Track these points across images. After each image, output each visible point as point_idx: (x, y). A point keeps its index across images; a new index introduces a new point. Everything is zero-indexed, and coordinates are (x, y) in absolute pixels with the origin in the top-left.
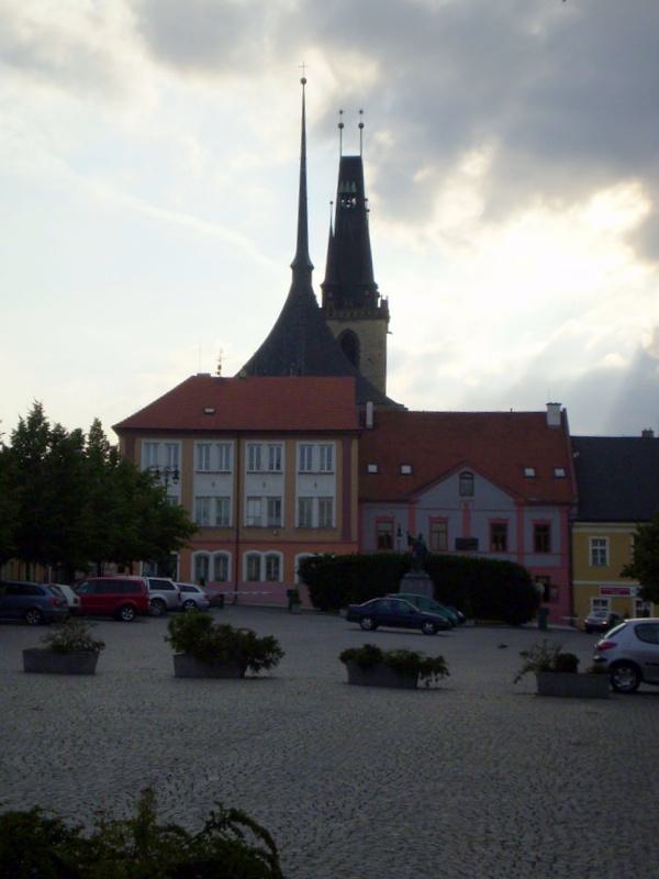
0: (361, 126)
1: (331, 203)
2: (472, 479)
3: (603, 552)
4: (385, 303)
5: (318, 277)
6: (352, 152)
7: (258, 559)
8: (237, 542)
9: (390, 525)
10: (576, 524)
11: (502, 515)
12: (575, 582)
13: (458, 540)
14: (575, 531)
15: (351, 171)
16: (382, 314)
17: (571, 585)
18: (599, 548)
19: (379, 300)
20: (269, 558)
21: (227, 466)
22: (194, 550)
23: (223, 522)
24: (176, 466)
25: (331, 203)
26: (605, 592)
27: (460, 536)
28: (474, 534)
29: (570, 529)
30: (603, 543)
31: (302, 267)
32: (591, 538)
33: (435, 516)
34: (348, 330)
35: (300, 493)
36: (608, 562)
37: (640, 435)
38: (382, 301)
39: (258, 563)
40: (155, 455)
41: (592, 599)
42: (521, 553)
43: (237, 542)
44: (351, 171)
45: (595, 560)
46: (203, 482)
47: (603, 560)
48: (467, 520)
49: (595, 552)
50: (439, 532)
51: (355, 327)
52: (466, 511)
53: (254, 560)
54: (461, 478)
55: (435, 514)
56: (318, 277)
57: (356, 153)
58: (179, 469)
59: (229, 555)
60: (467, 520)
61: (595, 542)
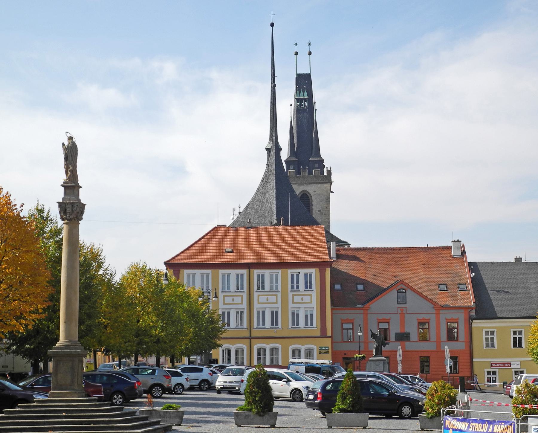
0: (310, 53)
1: (291, 105)
2: (405, 292)
3: (493, 339)
4: (329, 172)
5: (285, 155)
6: (304, 71)
7: (229, 351)
8: (250, 338)
9: (387, 324)
10: (474, 321)
11: (426, 317)
12: (474, 360)
13: (397, 334)
14: (473, 325)
15: (304, 82)
16: (328, 179)
17: (472, 362)
18: (517, 336)
19: (325, 170)
20: (271, 350)
21: (277, 288)
22: (220, 346)
23: (302, 323)
24: (208, 287)
25: (291, 105)
26: (493, 365)
27: (399, 331)
28: (407, 330)
29: (470, 325)
30: (520, 333)
31: (274, 149)
32: (512, 330)
33: (381, 318)
34: (304, 191)
35: (256, 306)
36: (496, 346)
37: (513, 260)
38: (328, 170)
39: (229, 354)
40: (194, 282)
41: (486, 370)
42: (439, 342)
43: (250, 338)
44: (304, 82)
45: (487, 345)
46: (228, 298)
47: (493, 345)
48: (402, 323)
49: (487, 339)
50: (348, 329)
51: (311, 189)
52: (402, 315)
53: (261, 352)
54: (398, 292)
55: (381, 317)
56: (285, 155)
57: (306, 71)
58: (210, 288)
59: (245, 348)
60: (402, 323)
61: (487, 333)
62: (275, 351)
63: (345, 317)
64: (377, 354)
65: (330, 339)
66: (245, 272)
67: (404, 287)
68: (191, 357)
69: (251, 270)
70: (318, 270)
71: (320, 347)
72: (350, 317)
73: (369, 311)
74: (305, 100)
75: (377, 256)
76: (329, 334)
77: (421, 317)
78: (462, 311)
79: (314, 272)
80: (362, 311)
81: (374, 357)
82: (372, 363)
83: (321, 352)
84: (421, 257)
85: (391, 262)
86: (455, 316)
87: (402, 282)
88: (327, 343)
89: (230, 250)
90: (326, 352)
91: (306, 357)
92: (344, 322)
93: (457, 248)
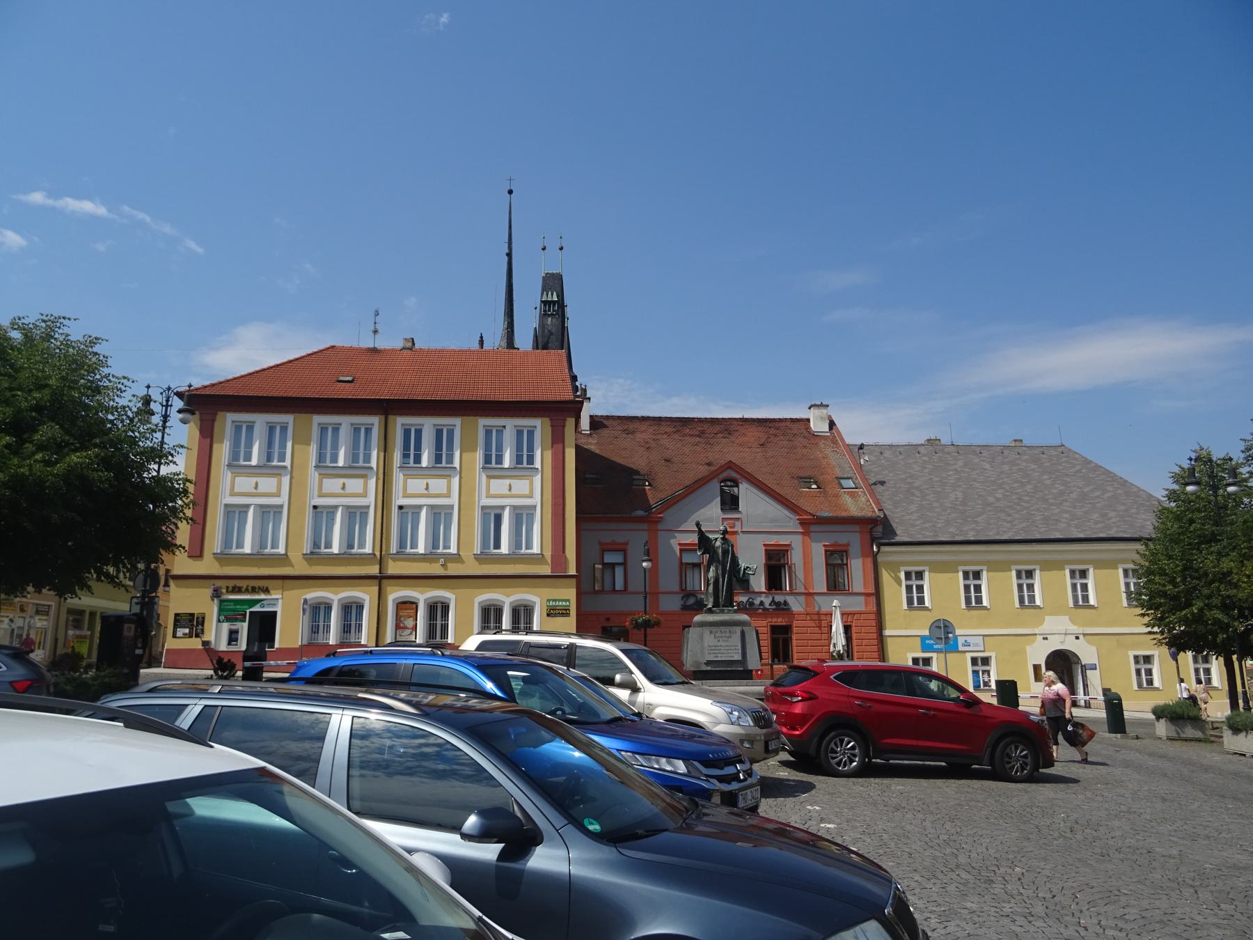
8: (381, 579)
11: (783, 540)
12: (887, 632)
43: (381, 579)
44: (553, 282)
62: (438, 611)
63: (608, 537)
64: (716, 604)
65: (574, 581)
66: (375, 421)
67: (735, 475)
68: (133, 626)
69: (391, 418)
70: (547, 421)
71: (549, 601)
72: (620, 537)
73: (660, 527)
74: (554, 302)
75: (669, 430)
76: (572, 571)
77: (772, 540)
78: (857, 528)
79: (539, 425)
80: (645, 526)
81: (710, 611)
82: (706, 631)
83: (552, 613)
84: (754, 434)
85: (698, 439)
86: (842, 539)
87: (730, 465)
88: (568, 594)
89: (350, 379)
90: (565, 613)
91: (515, 630)
92: (606, 548)
93: (822, 418)
